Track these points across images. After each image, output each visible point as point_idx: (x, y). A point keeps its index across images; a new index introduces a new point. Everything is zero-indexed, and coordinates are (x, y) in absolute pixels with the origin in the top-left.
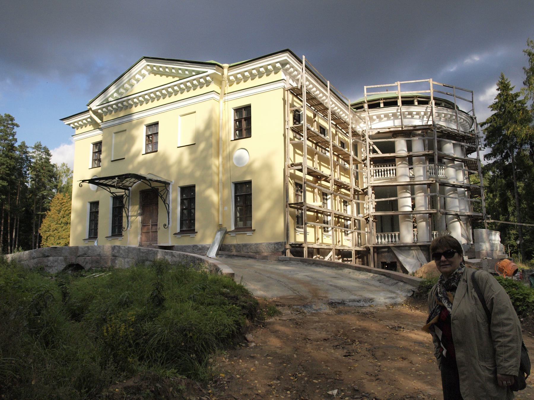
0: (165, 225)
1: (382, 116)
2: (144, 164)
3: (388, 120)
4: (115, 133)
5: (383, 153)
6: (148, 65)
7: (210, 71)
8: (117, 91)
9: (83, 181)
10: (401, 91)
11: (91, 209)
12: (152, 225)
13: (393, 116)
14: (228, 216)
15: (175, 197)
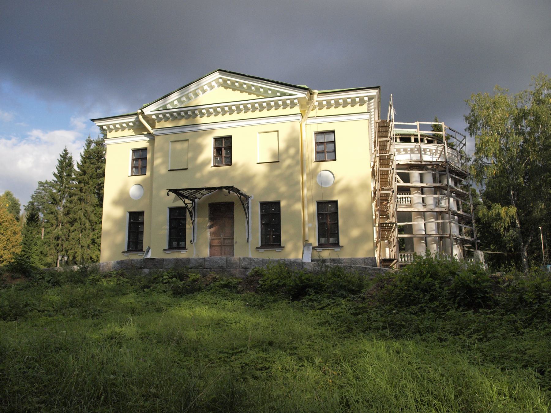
0: (191, 241)
1: (402, 150)
2: (212, 175)
3: (405, 154)
4: (171, 142)
5: (405, 182)
6: (221, 78)
7: (300, 94)
8: (179, 100)
9: (170, 190)
10: (420, 130)
11: (130, 220)
12: (224, 239)
13: (410, 151)
14: (122, 238)
15: (255, 212)
